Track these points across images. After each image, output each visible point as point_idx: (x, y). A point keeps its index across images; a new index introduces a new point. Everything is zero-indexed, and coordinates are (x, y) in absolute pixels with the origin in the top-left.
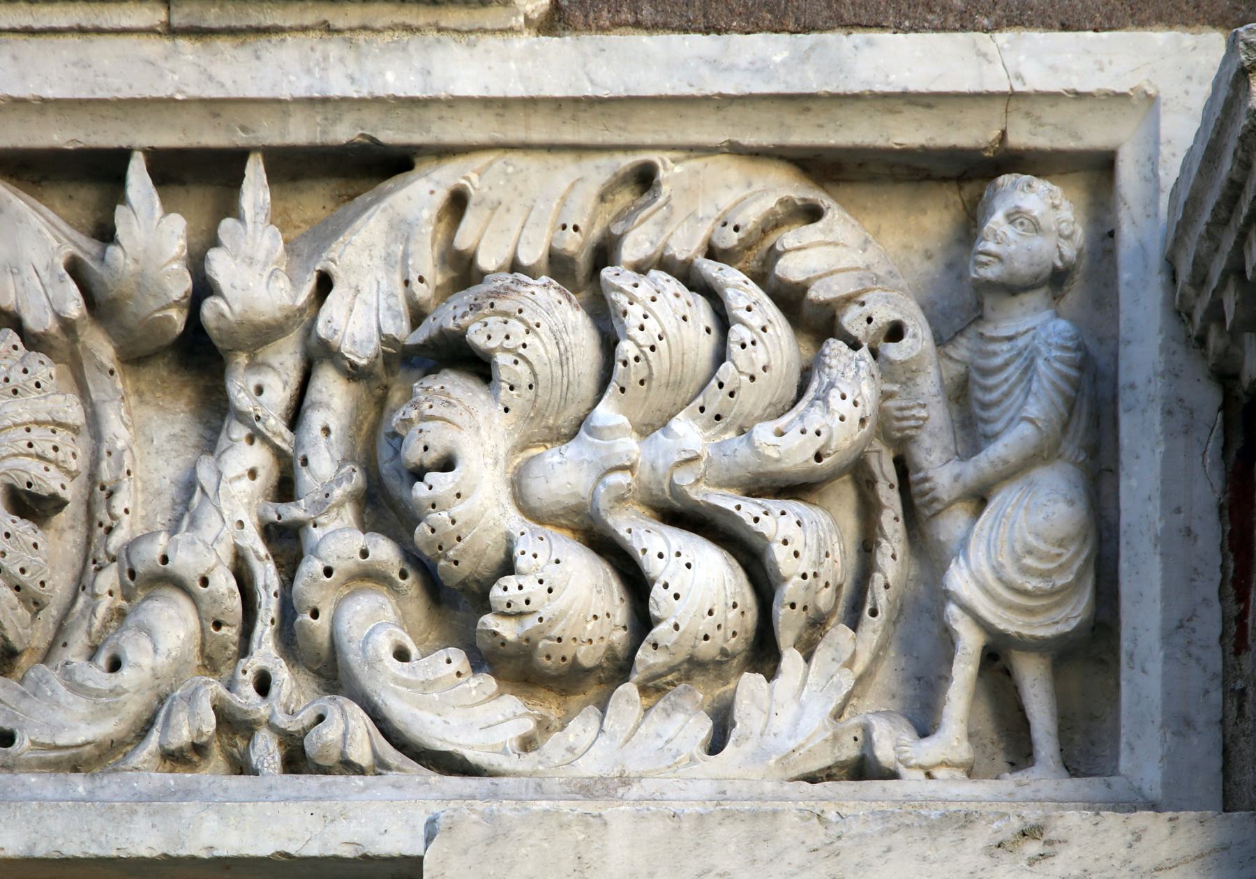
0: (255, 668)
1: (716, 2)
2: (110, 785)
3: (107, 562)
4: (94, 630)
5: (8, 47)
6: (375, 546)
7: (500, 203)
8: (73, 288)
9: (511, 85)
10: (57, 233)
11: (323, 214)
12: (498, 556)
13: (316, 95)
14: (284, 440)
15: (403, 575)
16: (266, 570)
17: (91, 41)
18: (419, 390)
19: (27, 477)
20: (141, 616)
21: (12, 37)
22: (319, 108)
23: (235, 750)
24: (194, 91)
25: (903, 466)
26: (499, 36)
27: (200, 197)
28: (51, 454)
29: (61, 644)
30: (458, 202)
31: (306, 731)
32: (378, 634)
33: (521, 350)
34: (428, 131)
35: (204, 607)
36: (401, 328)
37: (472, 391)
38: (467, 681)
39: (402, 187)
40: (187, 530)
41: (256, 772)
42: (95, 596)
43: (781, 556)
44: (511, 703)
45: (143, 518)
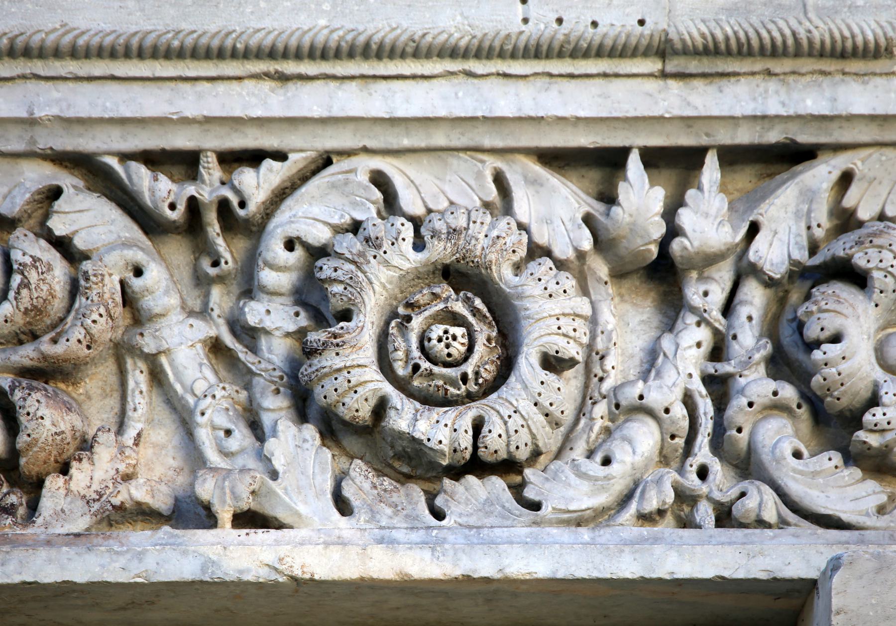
0: (698, 463)
1: (10, 1)
2: (605, 535)
3: (600, 399)
4: (591, 440)
5: (556, 86)
6: (783, 389)
7: (875, 179)
8: (587, 232)
9: (891, 107)
10: (578, 199)
11: (750, 186)
12: (866, 394)
13: (759, 114)
14: (721, 324)
15: (799, 406)
16: (706, 404)
17: (611, 82)
18: (817, 293)
19: (556, 348)
20: (625, 432)
21: (559, 79)
22: (759, 122)
23: (682, 513)
24: (677, 112)
26: (884, 77)
27: (670, 175)
28: (572, 334)
29: (568, 448)
30: (846, 179)
31: (732, 503)
32: (784, 442)
33: (890, 269)
34: (831, 135)
35: (665, 426)
36: (804, 255)
37: (854, 294)
38: (842, 471)
39: (809, 170)
40: (654, 379)
41: (700, 527)
42: (592, 419)
44: (871, 485)
45: (621, 371)
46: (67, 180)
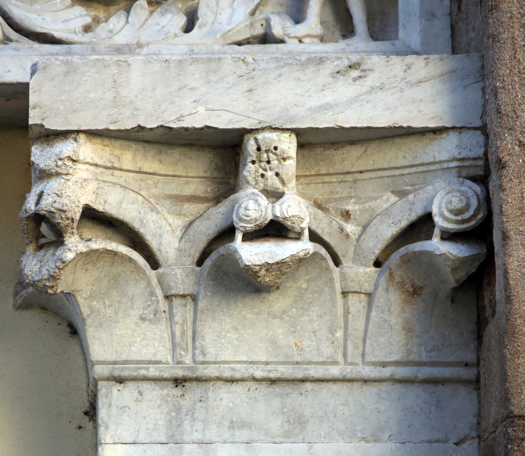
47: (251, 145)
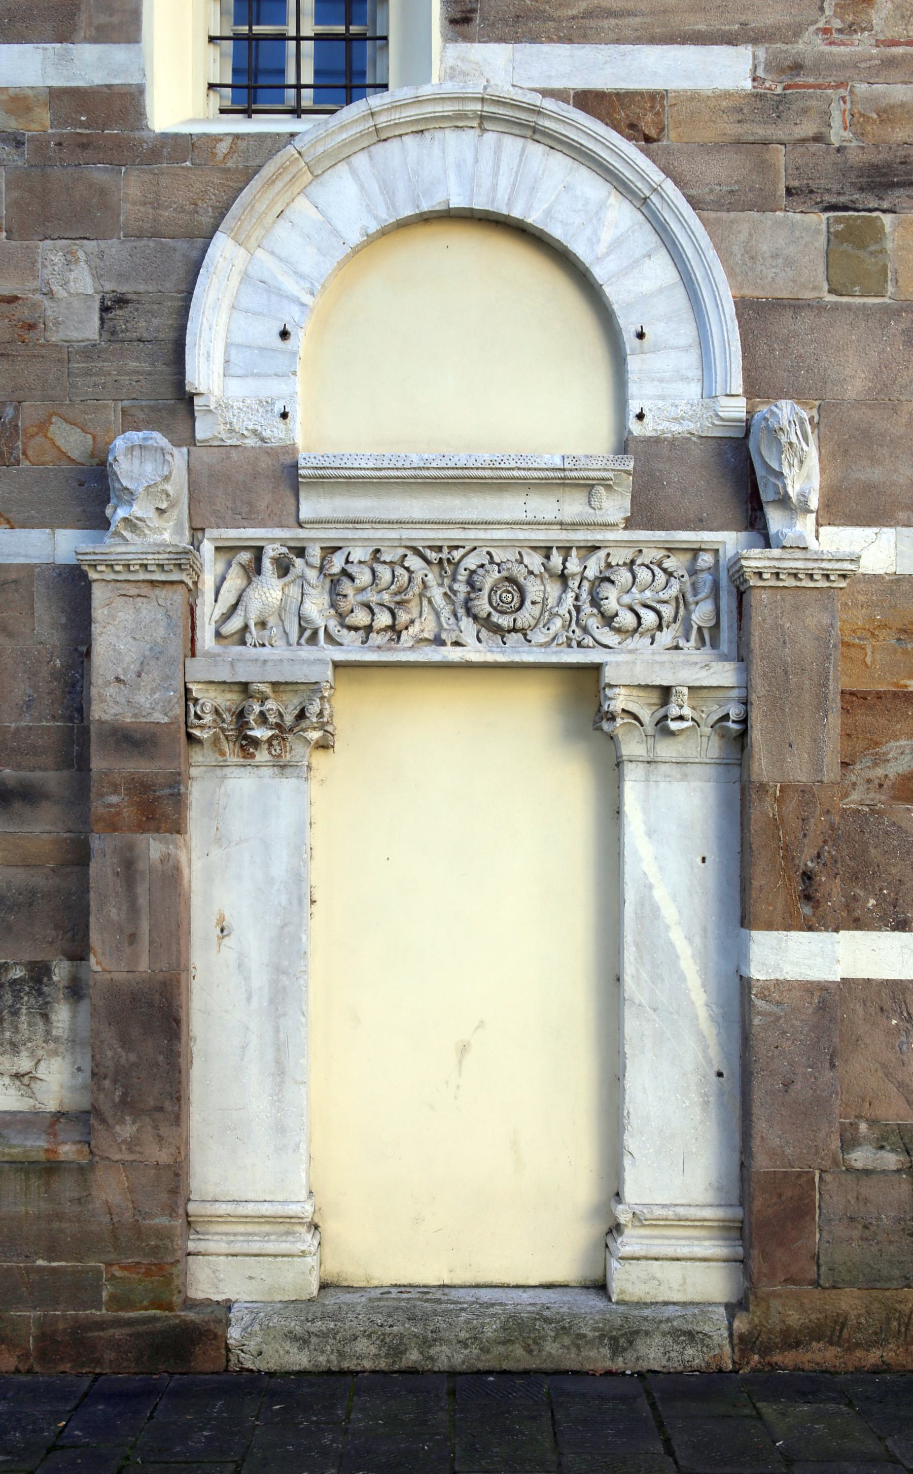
2: (548, 650)
25: (683, 596)
30: (608, 555)
43: (664, 614)
44: (617, 636)
46: (409, 553)
47: (674, 691)
